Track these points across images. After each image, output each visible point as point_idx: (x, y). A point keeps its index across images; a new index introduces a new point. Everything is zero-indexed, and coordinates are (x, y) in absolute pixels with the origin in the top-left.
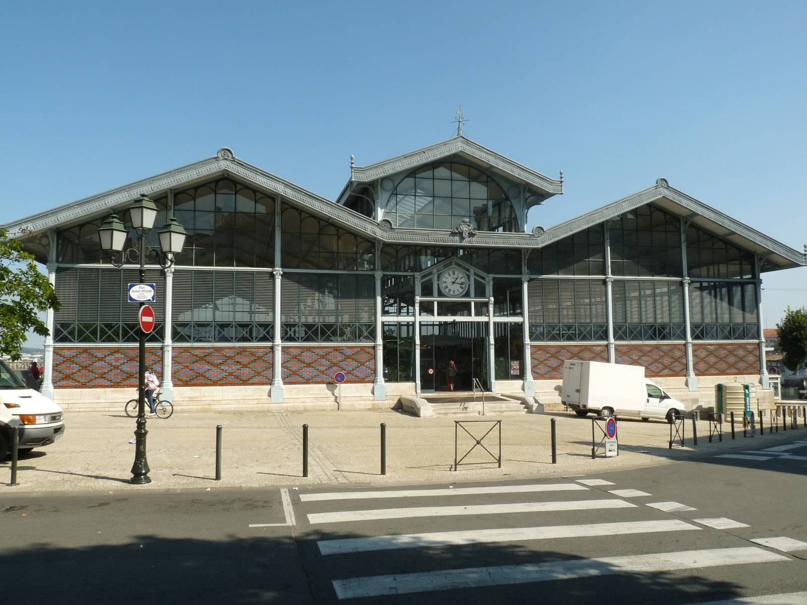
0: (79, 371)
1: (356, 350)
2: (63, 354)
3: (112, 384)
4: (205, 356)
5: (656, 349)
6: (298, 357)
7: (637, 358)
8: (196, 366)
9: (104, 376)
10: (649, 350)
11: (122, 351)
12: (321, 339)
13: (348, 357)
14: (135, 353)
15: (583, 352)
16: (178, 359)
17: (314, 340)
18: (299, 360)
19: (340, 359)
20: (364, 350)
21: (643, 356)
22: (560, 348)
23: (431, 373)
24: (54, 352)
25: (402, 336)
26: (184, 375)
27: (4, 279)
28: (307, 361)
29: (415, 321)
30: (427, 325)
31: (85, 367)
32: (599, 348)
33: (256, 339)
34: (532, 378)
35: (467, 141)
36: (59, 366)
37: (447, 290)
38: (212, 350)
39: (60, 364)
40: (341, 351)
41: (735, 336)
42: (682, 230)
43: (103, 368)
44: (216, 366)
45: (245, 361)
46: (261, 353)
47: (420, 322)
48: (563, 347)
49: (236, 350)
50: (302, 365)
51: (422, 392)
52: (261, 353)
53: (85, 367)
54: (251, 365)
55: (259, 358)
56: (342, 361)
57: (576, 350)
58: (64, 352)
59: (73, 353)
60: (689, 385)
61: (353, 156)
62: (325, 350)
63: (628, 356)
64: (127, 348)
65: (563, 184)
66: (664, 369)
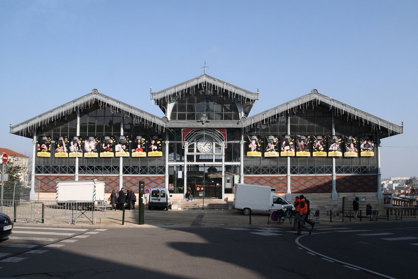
0: (44, 185)
1: (156, 178)
2: (38, 178)
5: (315, 178)
6: (130, 181)
7: (303, 183)
10: (310, 179)
12: (60, 172)
13: (152, 181)
14: (65, 178)
15: (273, 180)
16: (246, 182)
17: (342, 173)
18: (130, 182)
19: (149, 182)
20: (160, 178)
21: (307, 182)
22: (260, 178)
23: (198, 190)
24: (35, 178)
25: (199, 171)
27: (105, 146)
28: (134, 183)
29: (241, 164)
30: (202, 167)
32: (282, 178)
33: (158, 173)
34: (336, 192)
35: (208, 77)
37: (203, 150)
38: (157, 178)
40: (149, 179)
46: (114, 179)
47: (169, 165)
48: (262, 177)
50: (132, 185)
52: (114, 179)
54: (110, 184)
55: (113, 181)
56: (150, 183)
57: (269, 179)
60: (286, 198)
61: (151, 88)
63: (298, 182)
64: (62, 176)
65: (258, 95)
66: (319, 189)
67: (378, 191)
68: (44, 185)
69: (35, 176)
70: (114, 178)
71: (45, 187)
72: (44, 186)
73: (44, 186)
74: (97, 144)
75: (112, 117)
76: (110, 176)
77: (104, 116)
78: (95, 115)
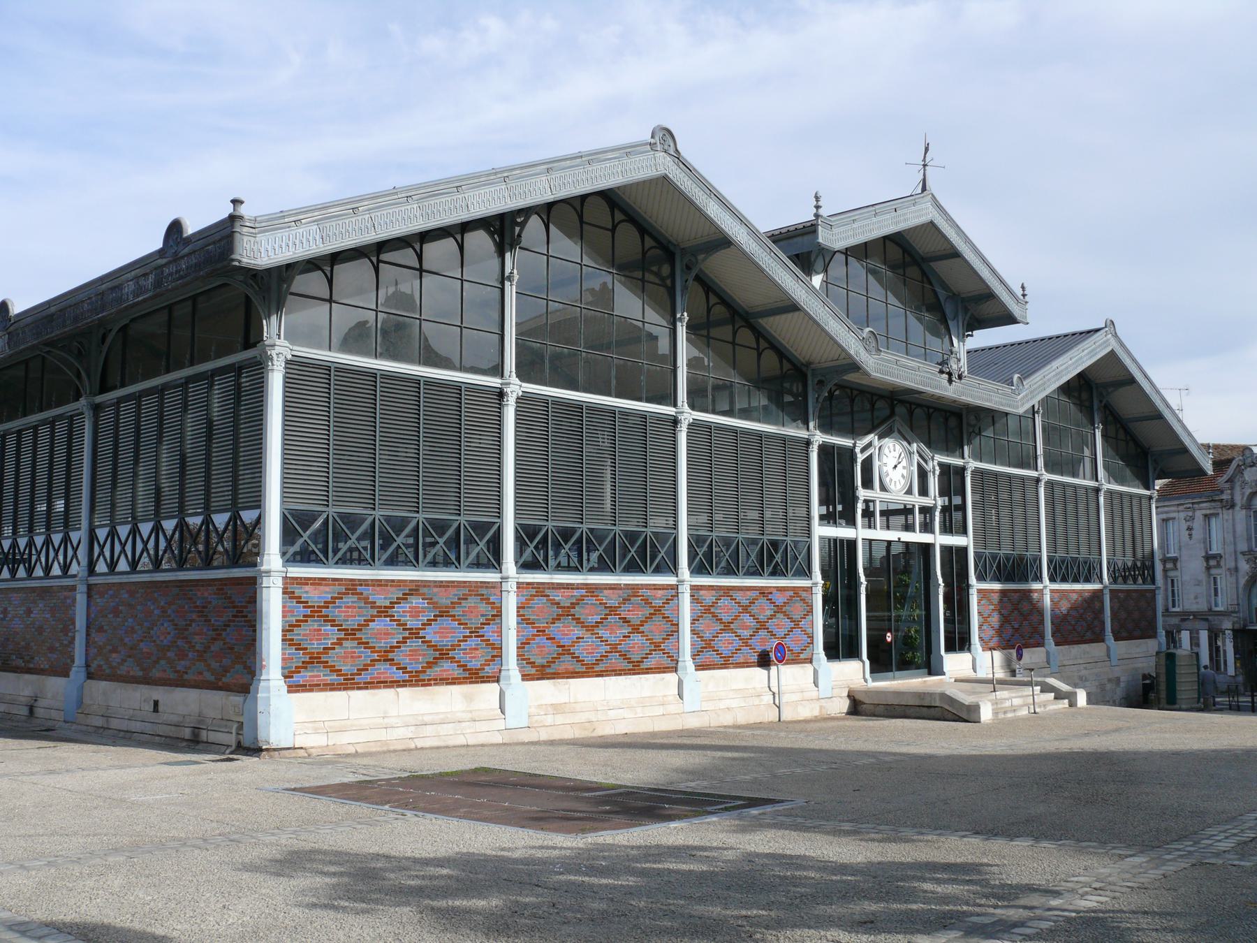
0: (339, 642)
2: (304, 597)
3: (407, 676)
4: (573, 605)
8: (557, 629)
9: (391, 656)
11: (425, 590)
26: (542, 651)
31: (350, 634)
36: (296, 630)
39: (298, 624)
41: (591, 565)
42: (1095, 407)
43: (388, 634)
44: (591, 628)
45: (636, 616)
49: (621, 592)
51: (874, 680)
53: (350, 634)
58: (307, 592)
59: (326, 593)
62: (748, 593)
67: (1158, 634)
68: (339, 642)
69: (285, 578)
71: (346, 657)
76: (648, 587)
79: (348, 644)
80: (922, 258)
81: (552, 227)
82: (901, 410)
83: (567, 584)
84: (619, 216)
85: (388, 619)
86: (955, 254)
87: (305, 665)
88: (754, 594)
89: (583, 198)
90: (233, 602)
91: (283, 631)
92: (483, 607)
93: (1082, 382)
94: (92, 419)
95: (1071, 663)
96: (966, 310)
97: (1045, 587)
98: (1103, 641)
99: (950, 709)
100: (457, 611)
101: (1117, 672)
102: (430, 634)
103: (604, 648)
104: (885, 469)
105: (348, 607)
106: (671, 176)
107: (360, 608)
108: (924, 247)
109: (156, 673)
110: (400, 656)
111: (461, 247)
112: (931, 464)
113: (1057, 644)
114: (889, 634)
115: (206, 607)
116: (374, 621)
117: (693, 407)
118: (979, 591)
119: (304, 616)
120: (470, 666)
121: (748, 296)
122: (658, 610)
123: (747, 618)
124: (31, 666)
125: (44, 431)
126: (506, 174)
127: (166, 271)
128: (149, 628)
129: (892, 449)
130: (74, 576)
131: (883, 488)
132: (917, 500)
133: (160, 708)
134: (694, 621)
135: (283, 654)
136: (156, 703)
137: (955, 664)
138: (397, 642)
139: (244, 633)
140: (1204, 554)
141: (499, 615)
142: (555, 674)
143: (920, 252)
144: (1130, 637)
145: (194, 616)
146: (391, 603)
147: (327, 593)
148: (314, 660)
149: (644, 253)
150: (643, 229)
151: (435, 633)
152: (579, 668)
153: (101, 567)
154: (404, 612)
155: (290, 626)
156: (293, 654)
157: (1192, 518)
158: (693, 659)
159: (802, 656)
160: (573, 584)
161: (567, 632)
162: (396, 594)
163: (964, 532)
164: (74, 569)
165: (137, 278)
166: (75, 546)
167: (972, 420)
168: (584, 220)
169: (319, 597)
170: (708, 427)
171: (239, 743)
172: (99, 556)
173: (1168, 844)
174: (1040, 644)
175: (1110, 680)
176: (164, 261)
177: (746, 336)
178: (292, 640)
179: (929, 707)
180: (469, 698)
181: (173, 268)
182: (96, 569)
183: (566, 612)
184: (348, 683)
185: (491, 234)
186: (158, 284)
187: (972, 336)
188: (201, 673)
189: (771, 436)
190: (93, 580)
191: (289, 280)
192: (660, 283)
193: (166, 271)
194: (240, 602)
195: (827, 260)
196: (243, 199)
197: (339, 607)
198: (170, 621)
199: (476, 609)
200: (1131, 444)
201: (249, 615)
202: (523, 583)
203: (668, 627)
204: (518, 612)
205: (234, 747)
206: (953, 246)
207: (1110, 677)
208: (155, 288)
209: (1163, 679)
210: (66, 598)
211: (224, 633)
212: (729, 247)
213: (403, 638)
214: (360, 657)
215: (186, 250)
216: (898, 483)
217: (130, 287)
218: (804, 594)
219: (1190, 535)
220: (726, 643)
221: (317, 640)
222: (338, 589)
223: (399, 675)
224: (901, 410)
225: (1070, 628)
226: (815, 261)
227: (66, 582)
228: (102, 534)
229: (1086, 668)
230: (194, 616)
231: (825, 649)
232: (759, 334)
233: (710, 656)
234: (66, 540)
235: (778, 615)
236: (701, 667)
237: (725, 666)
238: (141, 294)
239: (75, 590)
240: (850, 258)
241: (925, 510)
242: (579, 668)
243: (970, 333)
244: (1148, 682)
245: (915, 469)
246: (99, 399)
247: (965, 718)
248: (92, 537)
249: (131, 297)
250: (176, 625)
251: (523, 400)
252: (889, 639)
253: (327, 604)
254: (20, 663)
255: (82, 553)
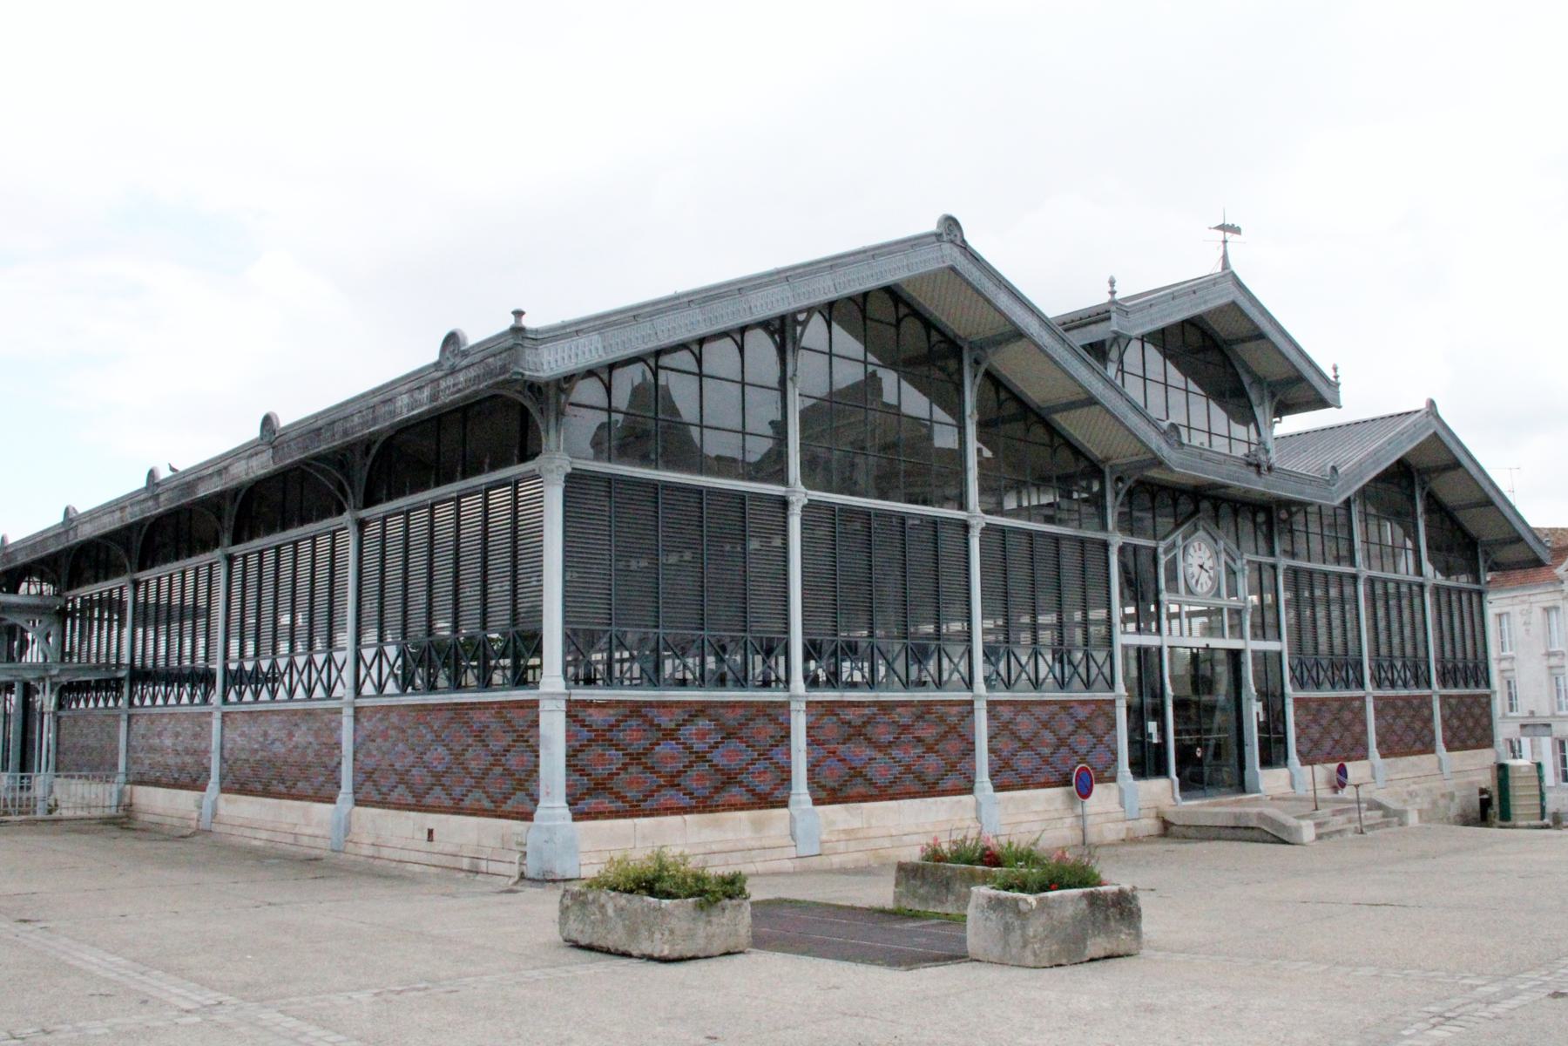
0: (625, 767)
3: (694, 803)
4: (865, 724)
9: (677, 781)
31: (636, 758)
36: (580, 756)
45: (929, 733)
49: (914, 709)
51: (1184, 798)
53: (636, 758)
58: (590, 715)
59: (610, 716)
69: (568, 701)
70: (955, 710)
71: (632, 782)
72: (623, 775)
73: (623, 775)
74: (1371, 510)
75: (747, 437)
77: (744, 433)
78: (709, 424)
79: (633, 769)
80: (1225, 342)
81: (834, 325)
82: (1205, 505)
83: (859, 702)
84: (903, 310)
85: (674, 742)
86: (1260, 336)
87: (590, 792)
88: (1055, 708)
89: (865, 295)
90: (512, 726)
91: (567, 756)
92: (771, 729)
93: (1402, 469)
94: (357, 535)
95: (1399, 776)
96: (1273, 395)
97: (1369, 694)
98: (1433, 752)
99: (1268, 830)
100: (745, 732)
101: (1450, 786)
102: (718, 758)
103: (897, 770)
104: (1190, 570)
105: (633, 730)
106: (958, 268)
107: (644, 730)
108: (1222, 329)
109: (429, 800)
110: (689, 781)
111: (741, 349)
112: (1239, 563)
113: (1383, 756)
114: (1198, 749)
115: (483, 731)
116: (659, 744)
117: (1122, 530)
118: (1296, 700)
119: (588, 740)
120: (758, 790)
121: (1037, 390)
122: (953, 728)
123: (1048, 736)
124: (293, 791)
125: (305, 547)
126: (788, 274)
127: (443, 384)
128: (421, 754)
129: (1197, 547)
130: (339, 698)
131: (1190, 591)
132: (1226, 602)
133: (435, 836)
134: (991, 738)
135: (567, 780)
136: (430, 832)
137: (1271, 781)
138: (684, 767)
139: (525, 758)
140: (1543, 651)
141: (788, 736)
142: (846, 797)
143: (1222, 334)
144: (1464, 747)
145: (470, 741)
146: (677, 725)
147: (610, 715)
148: (600, 787)
149: (930, 349)
150: (929, 324)
151: (722, 756)
152: (874, 792)
153: (368, 689)
154: (690, 734)
155: (574, 751)
156: (577, 780)
157: (1529, 612)
158: (992, 780)
159: (1106, 774)
160: (864, 702)
161: (860, 752)
162: (680, 715)
163: (1279, 637)
164: (339, 691)
165: (410, 391)
166: (340, 666)
167: (1284, 515)
168: (868, 314)
169: (605, 721)
170: (1003, 531)
171: (522, 874)
172: (322, 669)
173: (1522, 973)
174: (1364, 757)
175: (1443, 796)
176: (440, 374)
177: (1039, 433)
178: (577, 765)
179: (1247, 828)
180: (758, 826)
181: (450, 381)
182: (363, 691)
183: (856, 732)
184: (634, 810)
185: (772, 334)
186: (434, 397)
187: (1280, 422)
188: (479, 800)
189: (1043, 534)
190: (360, 702)
191: (567, 392)
192: (880, 363)
193: (443, 384)
194: (520, 726)
195: (1122, 348)
196: (524, 310)
197: (623, 730)
198: (444, 746)
199: (764, 730)
200: (1458, 533)
201: (531, 740)
202: (811, 702)
203: (963, 746)
204: (808, 732)
205: (517, 878)
206: (1257, 328)
207: (1443, 791)
208: (431, 401)
209: (1495, 794)
210: (331, 721)
211: (503, 759)
212: (1020, 340)
213: (690, 762)
214: (646, 782)
215: (465, 363)
216: (1204, 586)
217: (404, 400)
218: (1108, 708)
219: (1527, 630)
220: (1025, 762)
221: (602, 765)
222: (622, 710)
223: (686, 801)
224: (1205, 505)
225: (1396, 738)
226: (1110, 350)
227: (331, 704)
228: (368, 654)
229: (1415, 783)
230: (470, 741)
231: (1131, 765)
232: (1052, 430)
233: (1007, 776)
234: (329, 660)
235: (1080, 731)
236: (999, 788)
237: (1025, 785)
238: (416, 407)
239: (341, 713)
240: (1146, 344)
241: (1237, 613)
242: (874, 792)
243: (1278, 419)
244: (1485, 796)
245: (1223, 569)
246: (364, 513)
247: (1286, 839)
248: (358, 658)
249: (405, 410)
250: (451, 749)
251: (811, 507)
252: (1199, 755)
253: (611, 727)
254: (282, 788)
255: (348, 674)
